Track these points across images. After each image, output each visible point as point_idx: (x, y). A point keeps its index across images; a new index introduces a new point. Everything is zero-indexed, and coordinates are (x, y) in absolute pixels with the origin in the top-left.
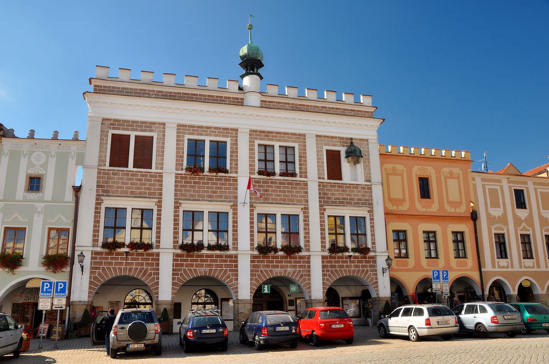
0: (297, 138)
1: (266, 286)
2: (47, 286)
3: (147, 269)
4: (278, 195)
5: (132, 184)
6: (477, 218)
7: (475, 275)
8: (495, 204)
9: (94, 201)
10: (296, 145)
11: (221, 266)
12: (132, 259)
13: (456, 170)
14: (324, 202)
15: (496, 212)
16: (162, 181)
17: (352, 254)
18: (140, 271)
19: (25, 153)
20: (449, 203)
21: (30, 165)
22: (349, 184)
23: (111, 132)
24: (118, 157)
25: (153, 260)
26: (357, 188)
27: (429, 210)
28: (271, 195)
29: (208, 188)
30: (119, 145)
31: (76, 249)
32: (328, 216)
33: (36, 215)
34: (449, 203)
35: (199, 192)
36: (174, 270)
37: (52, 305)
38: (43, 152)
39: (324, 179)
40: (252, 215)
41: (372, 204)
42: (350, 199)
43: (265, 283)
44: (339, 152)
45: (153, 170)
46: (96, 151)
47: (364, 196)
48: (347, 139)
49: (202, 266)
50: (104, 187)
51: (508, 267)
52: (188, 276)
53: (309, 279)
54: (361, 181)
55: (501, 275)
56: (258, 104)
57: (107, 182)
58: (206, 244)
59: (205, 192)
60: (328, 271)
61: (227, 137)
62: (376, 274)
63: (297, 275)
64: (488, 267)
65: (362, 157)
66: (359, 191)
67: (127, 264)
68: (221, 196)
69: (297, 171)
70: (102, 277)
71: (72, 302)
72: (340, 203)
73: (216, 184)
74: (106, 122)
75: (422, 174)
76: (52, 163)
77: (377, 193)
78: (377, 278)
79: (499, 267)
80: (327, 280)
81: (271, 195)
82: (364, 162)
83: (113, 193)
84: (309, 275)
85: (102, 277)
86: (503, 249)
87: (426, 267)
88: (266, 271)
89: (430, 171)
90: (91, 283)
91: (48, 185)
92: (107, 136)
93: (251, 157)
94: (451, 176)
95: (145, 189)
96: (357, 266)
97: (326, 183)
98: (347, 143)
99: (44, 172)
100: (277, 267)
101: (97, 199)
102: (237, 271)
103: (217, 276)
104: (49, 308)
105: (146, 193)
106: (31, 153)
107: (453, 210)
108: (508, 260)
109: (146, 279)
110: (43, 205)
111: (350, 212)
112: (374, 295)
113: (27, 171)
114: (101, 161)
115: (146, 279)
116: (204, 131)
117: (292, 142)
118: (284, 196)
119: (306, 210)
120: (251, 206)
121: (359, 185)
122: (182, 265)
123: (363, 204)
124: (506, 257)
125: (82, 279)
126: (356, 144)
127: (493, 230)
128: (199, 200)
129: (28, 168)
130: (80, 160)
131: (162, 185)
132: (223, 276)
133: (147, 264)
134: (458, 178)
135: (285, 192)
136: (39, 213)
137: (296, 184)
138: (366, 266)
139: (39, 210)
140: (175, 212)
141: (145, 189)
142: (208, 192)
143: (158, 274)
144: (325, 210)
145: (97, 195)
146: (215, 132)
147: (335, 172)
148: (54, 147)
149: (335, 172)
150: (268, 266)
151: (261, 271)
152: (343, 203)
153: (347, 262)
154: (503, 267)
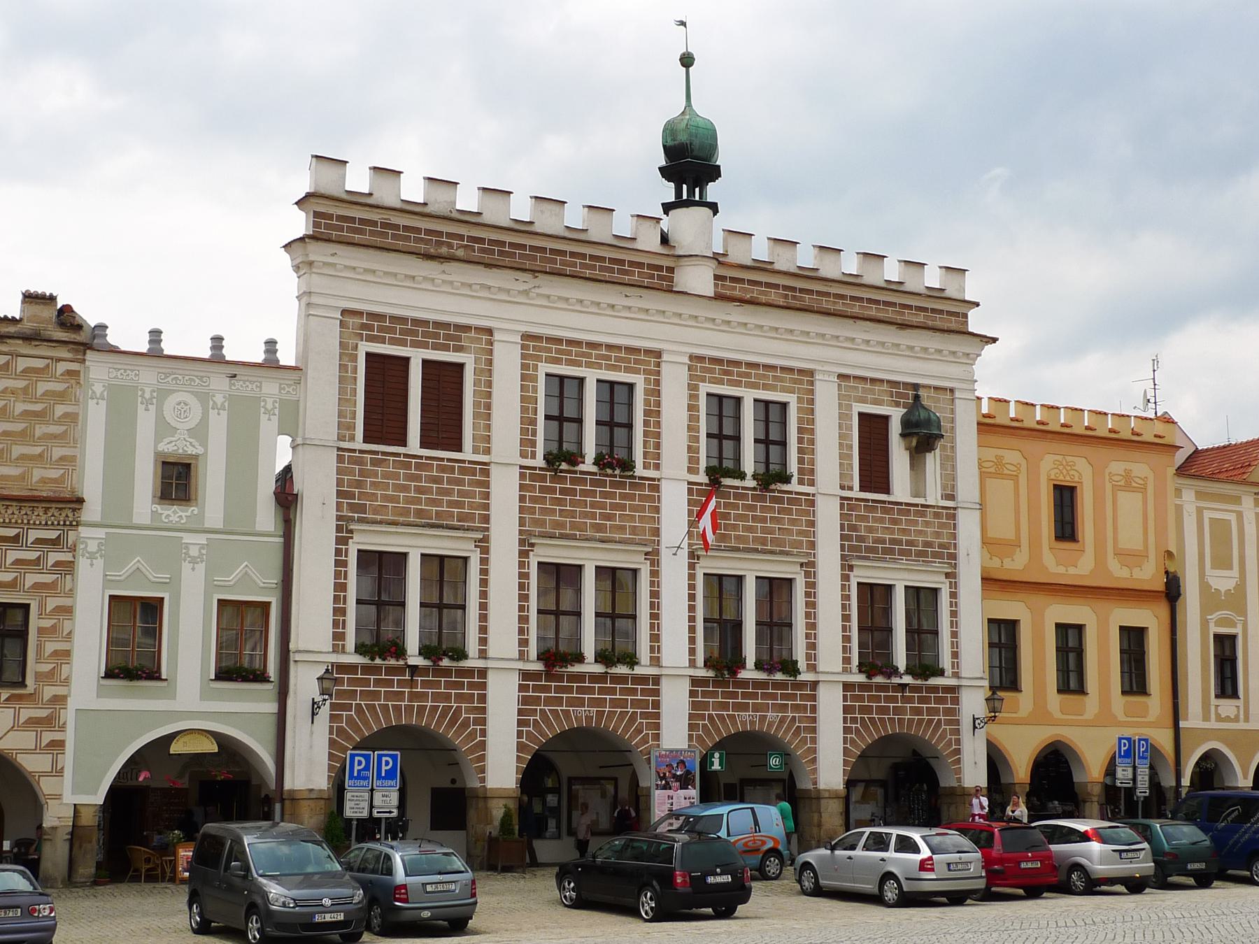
0: (795, 381)
1: (717, 755)
2: (360, 763)
3: (459, 709)
5: (419, 490)
6: (1179, 595)
7: (1164, 740)
8: (1222, 562)
9: (332, 535)
11: (623, 703)
12: (425, 684)
14: (851, 548)
15: (1223, 581)
16: (487, 485)
17: (907, 679)
18: (443, 715)
19: (147, 396)
21: (163, 428)
22: (907, 504)
23: (365, 347)
24: (384, 421)
25: (472, 686)
26: (923, 514)
27: (1072, 571)
28: (735, 527)
29: (593, 505)
30: (385, 376)
31: (293, 657)
33: (186, 567)
34: (1118, 554)
36: (520, 712)
37: (372, 807)
38: (192, 393)
39: (851, 488)
40: (692, 577)
41: (953, 557)
44: (886, 419)
45: (467, 454)
46: (331, 403)
47: (938, 535)
49: (581, 703)
50: (352, 496)
51: (1236, 719)
52: (550, 726)
53: (814, 740)
54: (933, 497)
55: (1218, 739)
57: (359, 484)
58: (1092, 767)
59: (585, 515)
60: (854, 720)
61: (637, 371)
62: (958, 732)
63: (789, 729)
64: (1192, 720)
66: (927, 524)
67: (414, 697)
68: (622, 528)
69: (793, 467)
70: (358, 730)
71: (292, 791)
72: (885, 551)
73: (612, 495)
74: (351, 321)
75: (1061, 478)
76: (218, 425)
77: (968, 529)
78: (958, 742)
79: (1219, 718)
80: (853, 741)
81: (735, 527)
83: (376, 511)
84: (814, 730)
85: (358, 730)
86: (1228, 674)
87: (1058, 715)
88: (721, 717)
89: (1078, 468)
90: (332, 743)
91: (212, 482)
92: (354, 358)
94: (1128, 484)
95: (451, 504)
96: (917, 711)
97: (857, 499)
98: (906, 396)
99: (200, 450)
100: (744, 707)
102: (658, 716)
103: (615, 729)
104: (365, 814)
105: (451, 515)
106: (163, 394)
108: (1240, 703)
109: (458, 734)
110: (202, 539)
111: (905, 575)
113: (156, 446)
114: (345, 428)
115: (458, 734)
116: (583, 355)
117: (784, 390)
119: (809, 567)
120: (692, 555)
121: (928, 506)
122: (537, 700)
124: (1235, 695)
125: (312, 733)
127: (1212, 625)
129: (158, 438)
130: (290, 423)
131: (487, 496)
132: (626, 729)
133: (460, 698)
135: (764, 520)
136: (194, 561)
137: (790, 501)
138: (423, 696)
139: (194, 552)
141: (451, 504)
142: (593, 516)
143: (483, 722)
144: (851, 568)
145: (339, 518)
146: (608, 358)
147: (875, 474)
149: (875, 474)
150: (724, 706)
152: (892, 551)
153: (894, 699)
154: (1228, 719)
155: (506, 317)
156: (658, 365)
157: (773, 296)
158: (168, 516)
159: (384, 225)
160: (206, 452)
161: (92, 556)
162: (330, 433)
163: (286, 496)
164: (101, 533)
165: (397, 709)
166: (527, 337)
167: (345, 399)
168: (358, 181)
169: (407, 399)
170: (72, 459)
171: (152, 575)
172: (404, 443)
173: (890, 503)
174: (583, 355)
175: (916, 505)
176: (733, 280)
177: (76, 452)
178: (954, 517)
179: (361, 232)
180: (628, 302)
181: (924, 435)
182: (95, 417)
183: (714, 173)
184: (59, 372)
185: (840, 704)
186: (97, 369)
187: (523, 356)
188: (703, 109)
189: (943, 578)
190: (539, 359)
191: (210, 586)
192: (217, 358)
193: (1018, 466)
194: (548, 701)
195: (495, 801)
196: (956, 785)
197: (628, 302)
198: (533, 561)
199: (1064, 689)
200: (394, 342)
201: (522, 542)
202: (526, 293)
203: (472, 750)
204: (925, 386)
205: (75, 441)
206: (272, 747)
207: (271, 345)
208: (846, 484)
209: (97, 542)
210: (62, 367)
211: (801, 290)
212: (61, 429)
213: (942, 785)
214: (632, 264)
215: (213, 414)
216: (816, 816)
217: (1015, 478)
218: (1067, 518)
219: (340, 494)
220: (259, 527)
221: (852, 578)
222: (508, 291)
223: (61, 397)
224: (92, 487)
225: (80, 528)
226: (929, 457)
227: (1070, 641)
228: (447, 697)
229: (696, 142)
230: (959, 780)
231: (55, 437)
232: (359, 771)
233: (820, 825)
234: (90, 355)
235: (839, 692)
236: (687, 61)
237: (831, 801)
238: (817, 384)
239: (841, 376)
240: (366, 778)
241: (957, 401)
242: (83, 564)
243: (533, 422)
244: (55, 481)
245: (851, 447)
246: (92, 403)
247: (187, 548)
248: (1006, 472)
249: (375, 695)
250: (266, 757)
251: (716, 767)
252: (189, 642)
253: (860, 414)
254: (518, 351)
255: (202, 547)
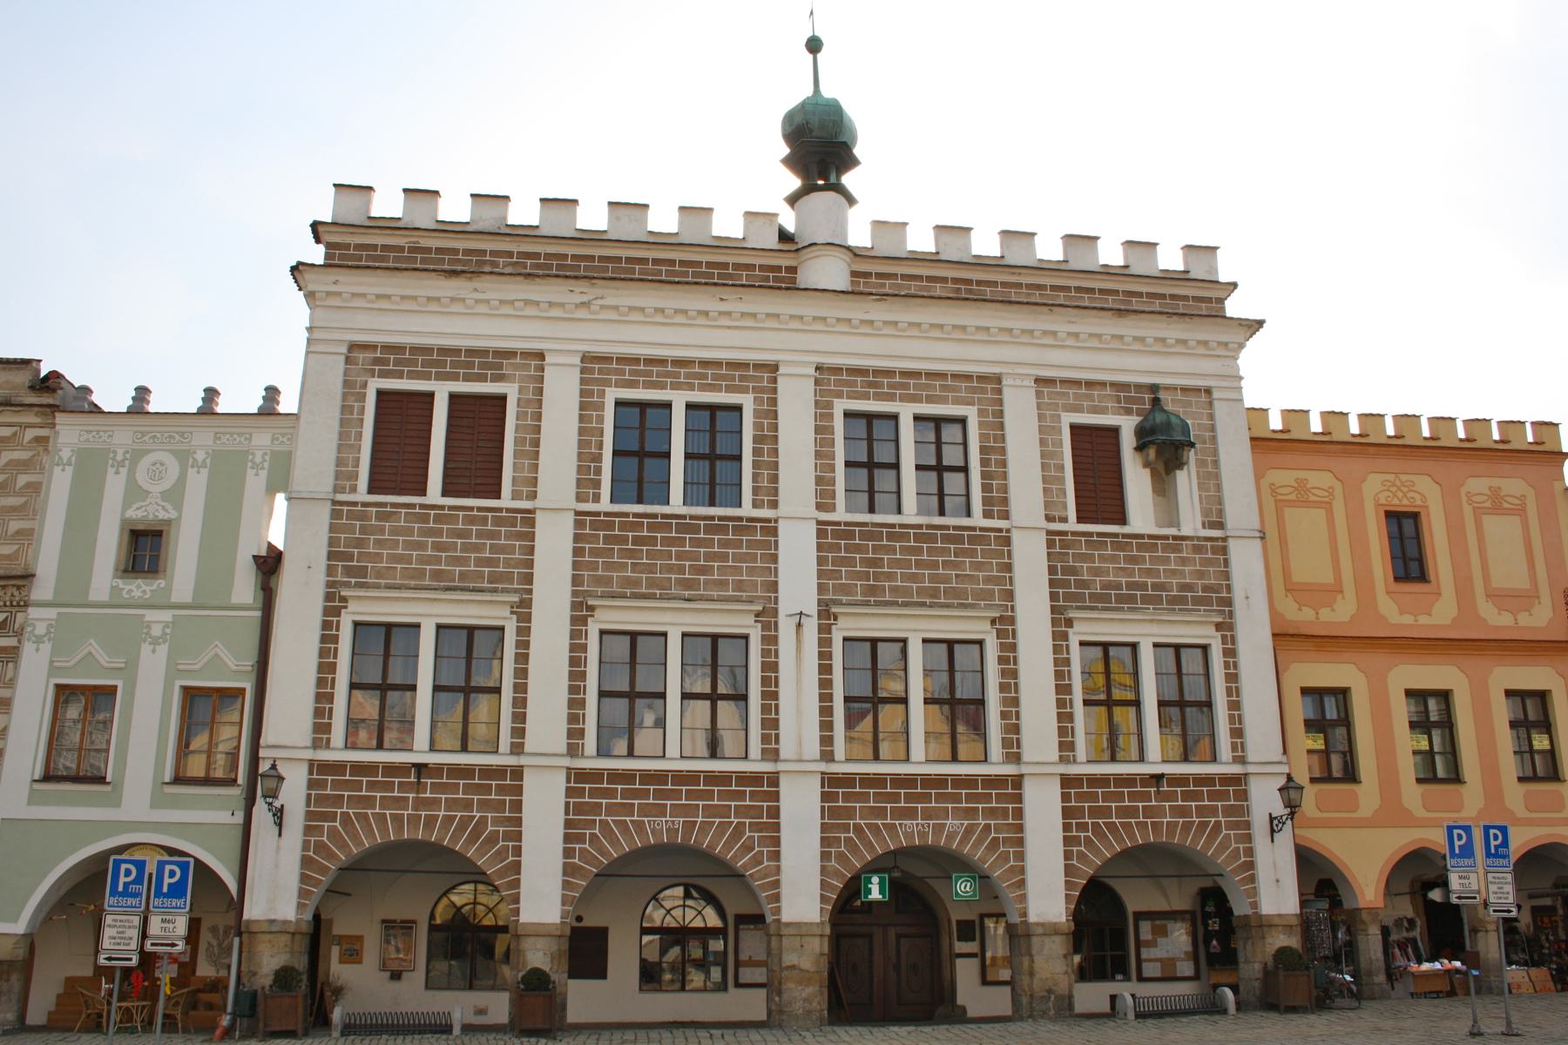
0: (974, 390)
1: (875, 880)
2: (128, 873)
3: (483, 820)
4: (914, 578)
5: (438, 547)
10: (971, 413)
12: (436, 788)
13: (1319, 480)
16: (531, 536)
19: (119, 457)
20: (1498, 597)
21: (134, 492)
22: (1150, 537)
23: (375, 384)
24: (396, 465)
26: (1177, 549)
27: (1424, 620)
30: (401, 418)
32: (1082, 644)
33: (146, 649)
35: (650, 569)
37: (144, 935)
39: (1064, 520)
41: (1228, 602)
42: (1156, 587)
43: (873, 868)
44: (1115, 431)
45: (506, 501)
48: (1139, 387)
52: (614, 842)
54: (1191, 523)
56: (841, 281)
57: (360, 543)
59: (670, 569)
60: (1082, 827)
61: (744, 390)
62: (1249, 838)
65: (1192, 445)
66: (1183, 561)
67: (420, 803)
68: (722, 584)
72: (1120, 599)
74: (361, 356)
75: (1396, 502)
76: (197, 483)
77: (1247, 567)
78: (1250, 852)
81: (890, 577)
82: (1201, 463)
83: (379, 575)
87: (1420, 812)
88: (875, 829)
89: (1422, 490)
90: (306, 862)
91: (184, 554)
93: (823, 454)
94: (1497, 505)
95: (479, 562)
96: (1183, 812)
97: (1074, 533)
98: (1141, 401)
99: (173, 514)
100: (910, 814)
101: (329, 597)
102: (777, 828)
103: (712, 846)
105: (480, 575)
106: (136, 456)
107: (1505, 620)
110: (167, 616)
112: (1240, 908)
114: (344, 477)
116: (668, 374)
117: (957, 401)
118: (933, 578)
119: (1005, 625)
123: (1198, 601)
125: (278, 848)
126: (1169, 402)
128: (652, 597)
129: (127, 503)
133: (484, 805)
134: (1521, 511)
136: (155, 642)
137: (972, 540)
138: (1213, 811)
139: (156, 631)
140: (574, 634)
142: (681, 569)
143: (518, 836)
144: (1069, 623)
147: (1100, 494)
148: (203, 439)
149: (1100, 494)
150: (881, 813)
151: (858, 828)
153: (1145, 797)
155: (561, 332)
156: (775, 381)
157: (938, 290)
158: (130, 591)
159: (413, 250)
160: (180, 517)
161: (39, 640)
162: (324, 484)
163: (269, 564)
164: (52, 613)
165: (398, 819)
166: (587, 358)
167: (347, 442)
168: (388, 205)
169: (426, 439)
170: (30, 532)
171: (103, 658)
172: (422, 491)
173: (1125, 536)
174: (668, 374)
175: (1166, 538)
176: (880, 275)
177: (35, 525)
178: (1224, 550)
179: (383, 258)
180: (724, 307)
181: (1167, 445)
182: (60, 485)
183: (849, 162)
184: (27, 439)
185: (1058, 805)
186: (69, 433)
187: (583, 381)
188: (827, 92)
189: (1211, 630)
190: (608, 383)
191: (172, 671)
192: (207, 409)
193: (1330, 491)
194: (611, 810)
195: (531, 940)
196: (1249, 912)
197: (724, 307)
198: (593, 629)
199: (1428, 777)
200: (414, 375)
201: (575, 606)
202: (585, 305)
203: (502, 873)
204: (1168, 388)
205: (35, 513)
206: (236, 868)
207: (272, 393)
208: (1057, 514)
209: (45, 624)
210: (30, 434)
211: (979, 283)
212: (21, 500)
213: (1236, 913)
214: (737, 266)
215: (191, 472)
216: (1026, 960)
217: (1328, 506)
218: (1412, 551)
219: (331, 556)
220: (235, 599)
221: (1071, 636)
222: (562, 305)
223: (25, 466)
224: (47, 565)
225: (30, 609)
226: (1181, 477)
227: (1432, 712)
228: (468, 805)
229: (815, 121)
230: (1255, 905)
231: (13, 509)
232: (126, 885)
233: (1031, 974)
234: (60, 418)
235: (1056, 790)
236: (814, 45)
237: (1047, 940)
238: (1006, 391)
239: (1038, 380)
240: (137, 895)
241: (1216, 403)
242: (28, 649)
243: (598, 458)
244: (8, 557)
245: (1061, 468)
246: (57, 470)
247: (148, 627)
248: (1312, 498)
249: (368, 802)
250: (233, 886)
251: (875, 894)
252: (144, 733)
253: (1073, 427)
254: (578, 375)
255: (166, 625)
